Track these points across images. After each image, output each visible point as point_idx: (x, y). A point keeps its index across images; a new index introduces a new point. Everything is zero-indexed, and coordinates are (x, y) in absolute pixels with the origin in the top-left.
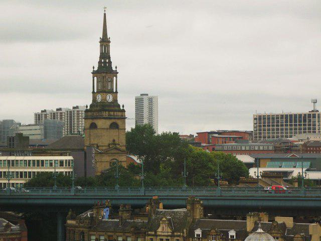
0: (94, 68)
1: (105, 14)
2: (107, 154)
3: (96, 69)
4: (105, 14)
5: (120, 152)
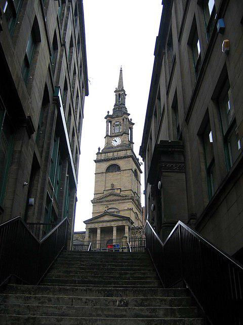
0: (108, 112)
1: (121, 70)
2: (101, 202)
3: (111, 113)
4: (121, 70)
5: (120, 198)
